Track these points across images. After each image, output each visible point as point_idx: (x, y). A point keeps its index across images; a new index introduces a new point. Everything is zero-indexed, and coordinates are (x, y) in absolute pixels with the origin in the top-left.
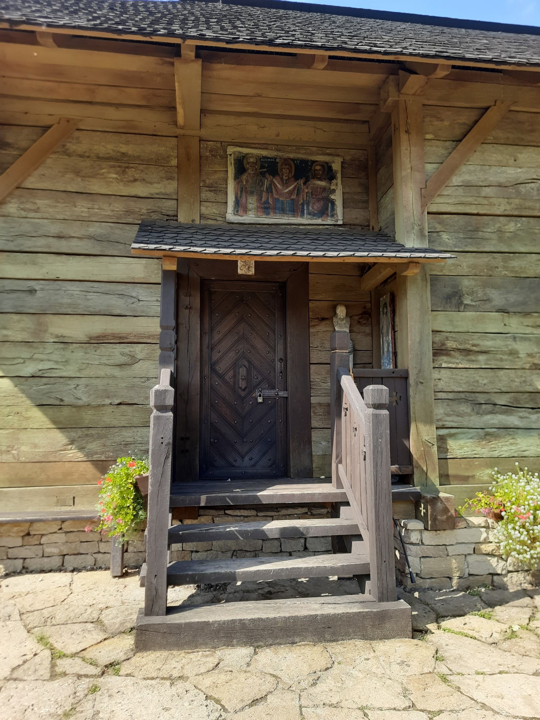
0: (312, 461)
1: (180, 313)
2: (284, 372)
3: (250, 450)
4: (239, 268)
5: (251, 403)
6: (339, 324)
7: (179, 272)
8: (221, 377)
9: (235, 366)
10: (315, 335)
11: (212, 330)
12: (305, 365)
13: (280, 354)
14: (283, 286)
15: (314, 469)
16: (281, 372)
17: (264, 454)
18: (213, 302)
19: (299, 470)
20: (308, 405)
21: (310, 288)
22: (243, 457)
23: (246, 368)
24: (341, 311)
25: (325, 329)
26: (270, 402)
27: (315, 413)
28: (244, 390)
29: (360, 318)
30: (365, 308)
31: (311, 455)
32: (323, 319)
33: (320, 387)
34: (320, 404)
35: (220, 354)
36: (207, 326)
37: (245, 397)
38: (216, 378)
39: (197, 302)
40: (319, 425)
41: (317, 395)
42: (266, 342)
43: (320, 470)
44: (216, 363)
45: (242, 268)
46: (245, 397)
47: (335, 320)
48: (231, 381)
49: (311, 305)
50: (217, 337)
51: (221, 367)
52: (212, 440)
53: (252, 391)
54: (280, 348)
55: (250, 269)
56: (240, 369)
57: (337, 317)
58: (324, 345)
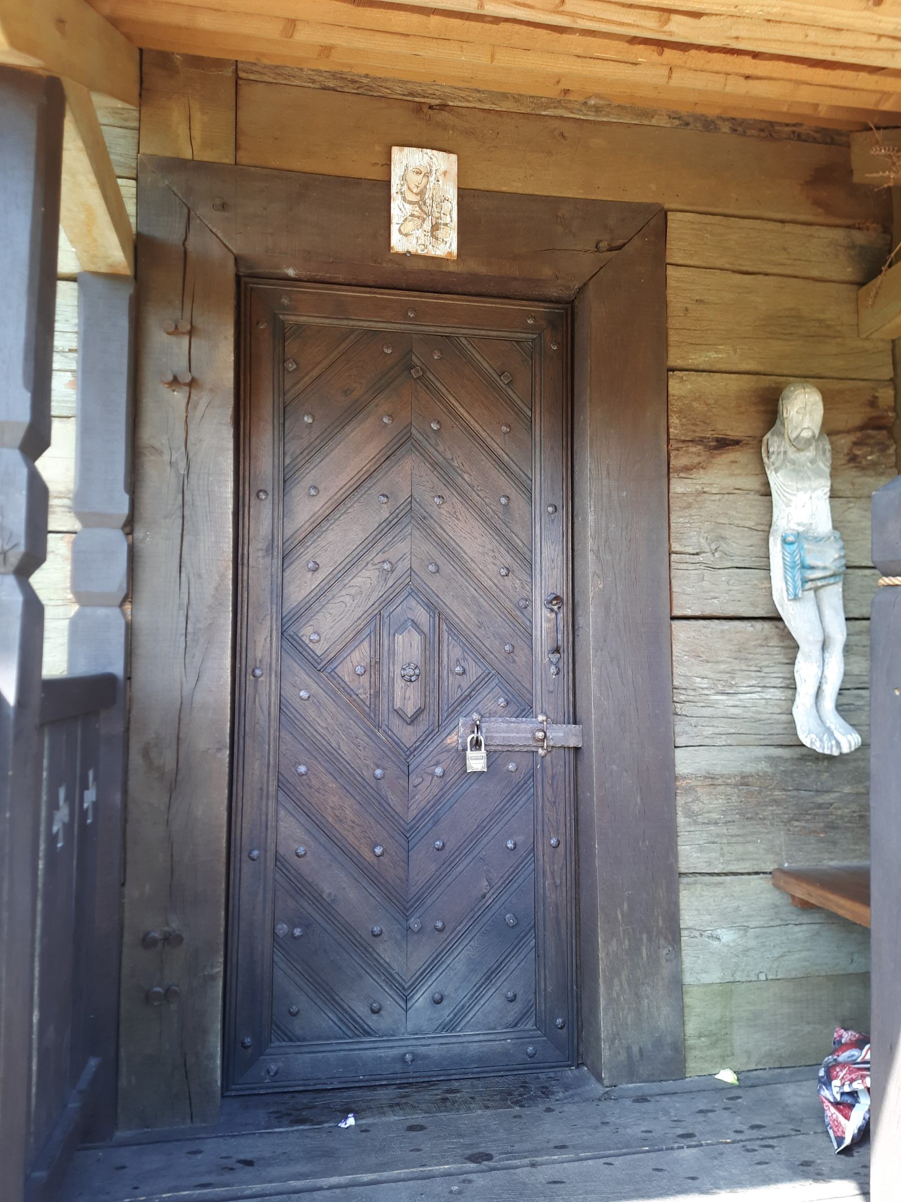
0: (681, 1010)
1: (149, 405)
2: (568, 649)
3: (432, 966)
4: (394, 229)
5: (438, 771)
6: (793, 463)
7: (145, 230)
8: (321, 667)
9: (377, 624)
10: (689, 506)
11: (286, 480)
12: (653, 620)
13: (549, 575)
14: (565, 316)
15: (690, 1042)
16: (557, 650)
17: (490, 976)
18: (291, 366)
19: (635, 1049)
20: (660, 785)
21: (673, 322)
22: (405, 995)
23: (421, 632)
24: (804, 410)
25: (730, 482)
26: (511, 767)
27: (690, 814)
28: (413, 720)
29: (855, 444)
30: (873, 403)
31: (677, 985)
32: (723, 444)
33: (708, 712)
34: (711, 779)
35: (320, 576)
36: (265, 463)
37: (413, 751)
38: (299, 674)
39: (219, 360)
40: (710, 864)
41: (698, 741)
42: (498, 532)
43: (713, 1045)
44: (306, 609)
45: (409, 227)
46: (413, 751)
47: (773, 442)
48: (362, 687)
49: (677, 387)
50: (305, 509)
51: (324, 630)
52: (282, 928)
53: (438, 728)
54: (549, 555)
55: (440, 234)
56: (399, 638)
57: (781, 435)
58: (724, 546)
